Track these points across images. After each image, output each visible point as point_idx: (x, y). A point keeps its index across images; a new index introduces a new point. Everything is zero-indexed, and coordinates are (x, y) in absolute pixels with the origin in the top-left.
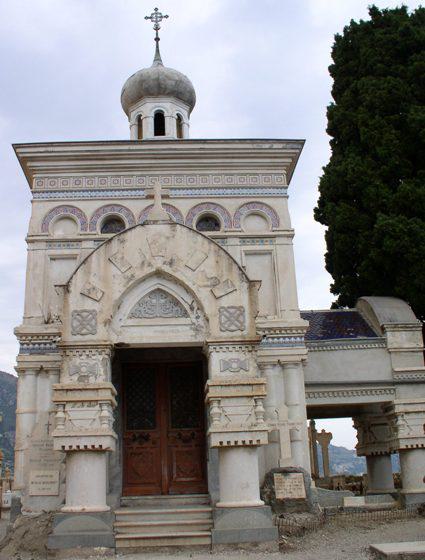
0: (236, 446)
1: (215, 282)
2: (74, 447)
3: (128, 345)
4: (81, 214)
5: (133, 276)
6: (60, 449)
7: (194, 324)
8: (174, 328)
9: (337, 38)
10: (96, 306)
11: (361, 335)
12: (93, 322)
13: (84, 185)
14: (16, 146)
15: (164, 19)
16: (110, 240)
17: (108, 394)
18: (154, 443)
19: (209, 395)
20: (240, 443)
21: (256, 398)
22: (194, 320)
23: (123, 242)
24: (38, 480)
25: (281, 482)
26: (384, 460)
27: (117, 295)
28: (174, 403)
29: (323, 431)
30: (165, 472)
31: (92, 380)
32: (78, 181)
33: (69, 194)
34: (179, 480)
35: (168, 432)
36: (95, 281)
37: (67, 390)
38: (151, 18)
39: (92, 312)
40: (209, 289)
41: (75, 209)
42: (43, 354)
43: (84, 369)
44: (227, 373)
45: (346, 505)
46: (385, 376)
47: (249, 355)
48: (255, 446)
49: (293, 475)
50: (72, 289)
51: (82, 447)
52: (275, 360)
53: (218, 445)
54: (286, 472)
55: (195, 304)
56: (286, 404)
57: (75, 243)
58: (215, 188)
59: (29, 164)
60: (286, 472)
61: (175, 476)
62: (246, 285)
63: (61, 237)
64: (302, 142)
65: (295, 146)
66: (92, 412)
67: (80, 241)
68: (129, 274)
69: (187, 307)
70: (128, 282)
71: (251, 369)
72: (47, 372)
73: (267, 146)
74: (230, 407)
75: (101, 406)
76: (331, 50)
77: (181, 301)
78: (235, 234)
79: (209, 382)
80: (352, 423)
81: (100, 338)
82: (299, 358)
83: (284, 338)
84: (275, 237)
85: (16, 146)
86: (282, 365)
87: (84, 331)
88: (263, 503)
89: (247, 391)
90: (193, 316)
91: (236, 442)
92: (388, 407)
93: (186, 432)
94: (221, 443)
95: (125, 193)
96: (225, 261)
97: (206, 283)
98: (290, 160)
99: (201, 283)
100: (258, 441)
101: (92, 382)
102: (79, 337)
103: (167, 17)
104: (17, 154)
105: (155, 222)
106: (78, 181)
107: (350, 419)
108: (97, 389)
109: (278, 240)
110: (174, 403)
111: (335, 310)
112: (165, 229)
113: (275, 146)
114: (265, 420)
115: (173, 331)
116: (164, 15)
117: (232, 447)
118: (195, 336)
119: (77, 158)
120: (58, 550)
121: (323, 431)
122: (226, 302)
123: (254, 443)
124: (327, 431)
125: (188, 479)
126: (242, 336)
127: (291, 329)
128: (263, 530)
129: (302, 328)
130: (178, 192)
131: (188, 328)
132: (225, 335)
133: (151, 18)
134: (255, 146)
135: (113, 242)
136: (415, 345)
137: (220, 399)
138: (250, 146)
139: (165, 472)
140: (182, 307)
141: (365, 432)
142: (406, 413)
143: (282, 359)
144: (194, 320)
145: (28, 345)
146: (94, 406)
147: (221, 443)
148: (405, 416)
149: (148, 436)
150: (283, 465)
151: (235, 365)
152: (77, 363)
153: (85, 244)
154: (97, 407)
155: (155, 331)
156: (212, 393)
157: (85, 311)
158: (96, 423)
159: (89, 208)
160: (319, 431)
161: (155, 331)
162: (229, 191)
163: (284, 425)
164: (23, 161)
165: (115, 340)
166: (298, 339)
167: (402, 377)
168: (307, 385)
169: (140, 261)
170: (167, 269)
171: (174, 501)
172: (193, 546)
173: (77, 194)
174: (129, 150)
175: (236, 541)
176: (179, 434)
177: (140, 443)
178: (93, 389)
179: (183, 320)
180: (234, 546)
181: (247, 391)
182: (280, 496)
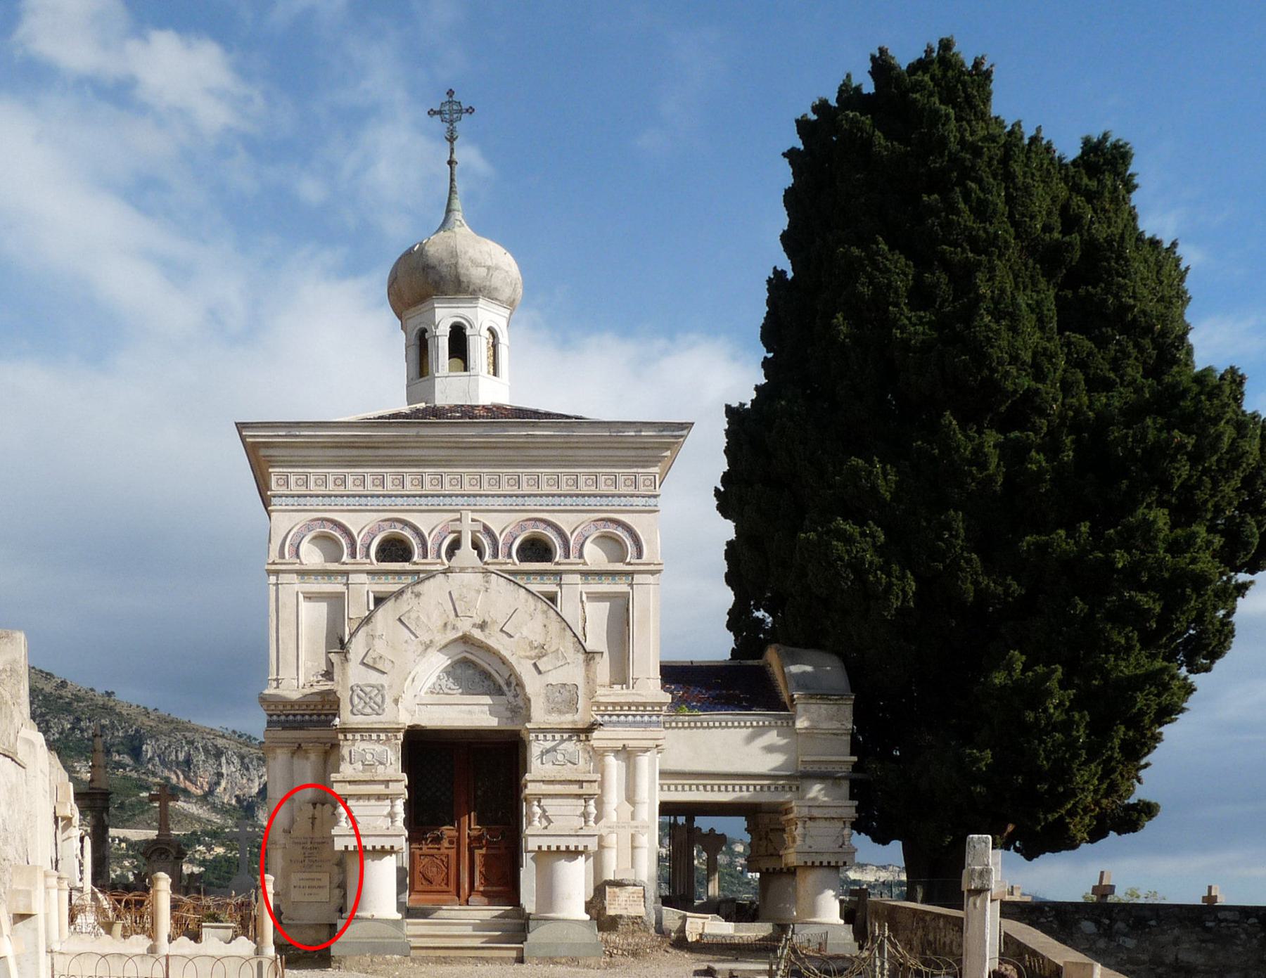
0: (813, 866)
1: (541, 651)
9: (791, 155)
13: (351, 488)
14: (241, 426)
15: (465, 116)
16: (401, 592)
17: (401, 787)
19: (527, 791)
21: (586, 798)
22: (511, 699)
23: (418, 595)
24: (302, 883)
25: (615, 896)
26: (785, 880)
36: (380, 647)
38: (440, 112)
39: (380, 688)
42: (301, 729)
43: (369, 757)
45: (706, 931)
47: (580, 746)
49: (630, 889)
52: (620, 744)
54: (619, 884)
59: (263, 452)
60: (619, 884)
62: (581, 657)
64: (687, 426)
69: (501, 682)
71: (582, 761)
74: (551, 806)
76: (785, 177)
77: (493, 673)
78: (574, 567)
79: (528, 776)
80: (745, 824)
85: (241, 426)
88: (588, 917)
89: (574, 789)
90: (510, 695)
94: (540, 847)
96: (555, 626)
97: (528, 654)
99: (522, 654)
101: (381, 772)
102: (360, 718)
103: (470, 110)
104: (243, 438)
105: (462, 570)
110: (479, 793)
111: (736, 662)
114: (602, 825)
116: (465, 106)
119: (337, 446)
120: (344, 957)
121: (712, 830)
122: (555, 678)
126: (574, 722)
127: (644, 705)
128: (586, 945)
132: (555, 720)
133: (440, 112)
135: (405, 596)
140: (495, 682)
143: (631, 744)
144: (511, 699)
147: (540, 847)
148: (809, 824)
156: (531, 789)
159: (359, 523)
164: (252, 450)
165: (406, 720)
168: (663, 774)
169: (441, 623)
170: (477, 634)
172: (502, 958)
180: (552, 960)
181: (574, 789)
182: (611, 911)
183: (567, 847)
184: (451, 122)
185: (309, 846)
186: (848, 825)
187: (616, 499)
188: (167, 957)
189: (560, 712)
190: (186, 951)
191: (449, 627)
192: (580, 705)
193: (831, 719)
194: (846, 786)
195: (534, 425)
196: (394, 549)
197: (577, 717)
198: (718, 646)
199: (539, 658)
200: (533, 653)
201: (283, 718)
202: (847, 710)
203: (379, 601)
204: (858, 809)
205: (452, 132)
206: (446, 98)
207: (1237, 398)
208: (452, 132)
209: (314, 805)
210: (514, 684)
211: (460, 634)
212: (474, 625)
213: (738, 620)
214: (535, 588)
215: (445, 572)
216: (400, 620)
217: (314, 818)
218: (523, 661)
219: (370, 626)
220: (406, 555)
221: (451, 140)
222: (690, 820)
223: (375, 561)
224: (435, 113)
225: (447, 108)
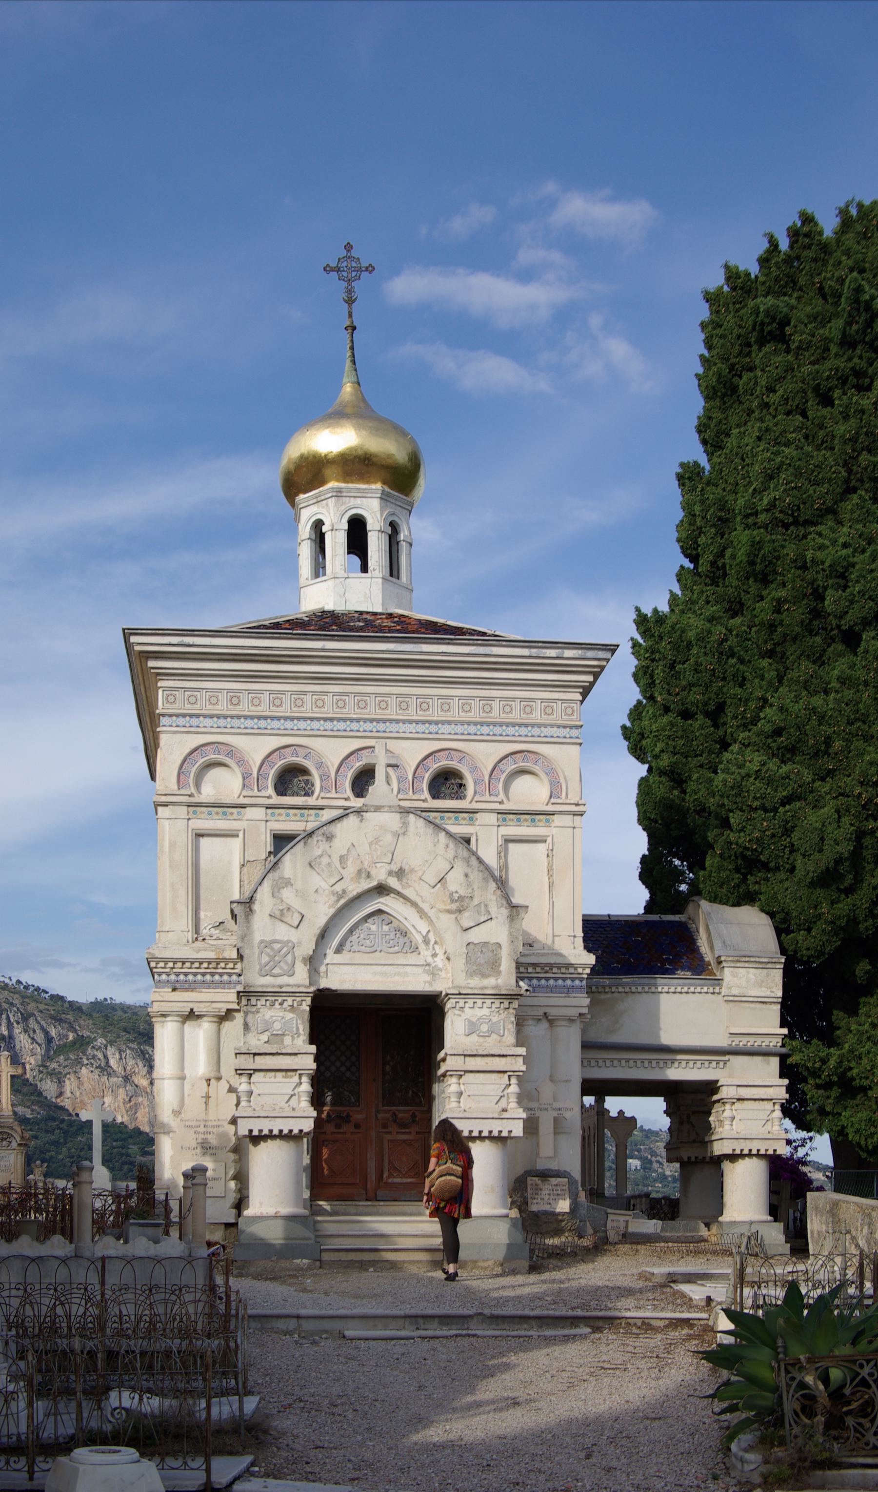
2: (266, 1132)
3: (336, 991)
4: (242, 762)
5: (344, 892)
6: (247, 1133)
7: (428, 965)
8: (402, 970)
10: (293, 935)
11: (683, 969)
12: (289, 958)
13: (245, 708)
18: (357, 1126)
20: (276, 1132)
22: (430, 959)
25: (538, 1189)
27: (322, 921)
28: (388, 1068)
29: (621, 1112)
30: (372, 1166)
31: (287, 1040)
32: (234, 698)
33: (222, 722)
34: (390, 1180)
35: (377, 1112)
37: (255, 1054)
38: (338, 270)
40: (453, 916)
41: (231, 750)
42: (193, 990)
43: (277, 1026)
44: (474, 1038)
45: (631, 1229)
46: (722, 1041)
48: (505, 1138)
49: (554, 1181)
50: (256, 907)
51: (276, 1132)
53: (731, 1152)
55: (431, 936)
56: (551, 1080)
57: (235, 810)
58: (462, 723)
60: (545, 1175)
61: (386, 1175)
62: (505, 912)
63: (212, 800)
64: (618, 646)
65: (601, 654)
66: (286, 1085)
67: (243, 806)
68: (338, 888)
69: (419, 939)
70: (338, 901)
72: (199, 1017)
73: (553, 653)
75: (300, 1078)
81: (299, 982)
82: (574, 1012)
83: (556, 979)
84: (553, 814)
86: (550, 1021)
87: (277, 971)
91: (480, 1132)
92: (712, 1087)
93: (404, 1112)
95: (316, 725)
97: (448, 907)
98: (590, 678)
99: (442, 907)
100: (510, 1132)
102: (268, 980)
104: (128, 646)
105: (378, 809)
106: (234, 698)
107: (662, 1099)
108: (296, 1054)
109: (557, 820)
110: (388, 1068)
111: (654, 917)
112: (392, 820)
113: (568, 653)
115: (399, 974)
116: (365, 264)
117: (746, 1155)
118: (430, 984)
121: (621, 1112)
123: (505, 1134)
124: (628, 1114)
125: (409, 1180)
126: (496, 987)
129: (584, 966)
130: (402, 727)
131: (420, 970)
132: (476, 983)
133: (338, 270)
134: (534, 652)
135: (315, 838)
136: (768, 993)
137: (461, 1074)
138: (525, 652)
139: (372, 1166)
141: (681, 1123)
142: (739, 1100)
143: (553, 1012)
145: (168, 975)
146: (291, 1077)
147: (251, 1131)
149: (348, 1116)
150: (541, 1165)
151: (484, 1028)
152: (267, 1017)
153: (250, 813)
154: (296, 1079)
155: (375, 973)
157: (276, 941)
158: (288, 1100)
160: (614, 1114)
161: (375, 973)
162: (485, 730)
163: (546, 1109)
166: (577, 982)
167: (742, 1042)
170: (393, 882)
171: (385, 1209)
173: (236, 723)
174: (323, 650)
175: (474, 1258)
176: (394, 1115)
177: (338, 1126)
178: (290, 1054)
179: (412, 959)
183: (281, 1131)
184: (349, 281)
185: (202, 1129)
186: (778, 1107)
187: (394, 725)
188: (103, 1259)
189: (484, 976)
190: (60, 1253)
191: (363, 875)
192: (503, 968)
193: (761, 986)
194: (775, 1062)
195: (449, 642)
196: (291, 778)
197: (500, 981)
198: (631, 899)
199: (460, 911)
200: (454, 906)
201: (173, 977)
202: (776, 977)
203: (282, 841)
204: (789, 1089)
205: (350, 291)
206: (344, 253)
207: (659, 618)
208: (350, 291)
209: (208, 1080)
210: (432, 942)
211: (374, 883)
212: (390, 873)
213: (651, 871)
214: (453, 829)
215: (359, 812)
216: (310, 864)
217: (208, 1097)
218: (441, 915)
219: (278, 871)
220: (459, 789)
221: (350, 301)
222: (600, 1101)
223: (349, 793)
224: (332, 270)
225: (345, 264)
